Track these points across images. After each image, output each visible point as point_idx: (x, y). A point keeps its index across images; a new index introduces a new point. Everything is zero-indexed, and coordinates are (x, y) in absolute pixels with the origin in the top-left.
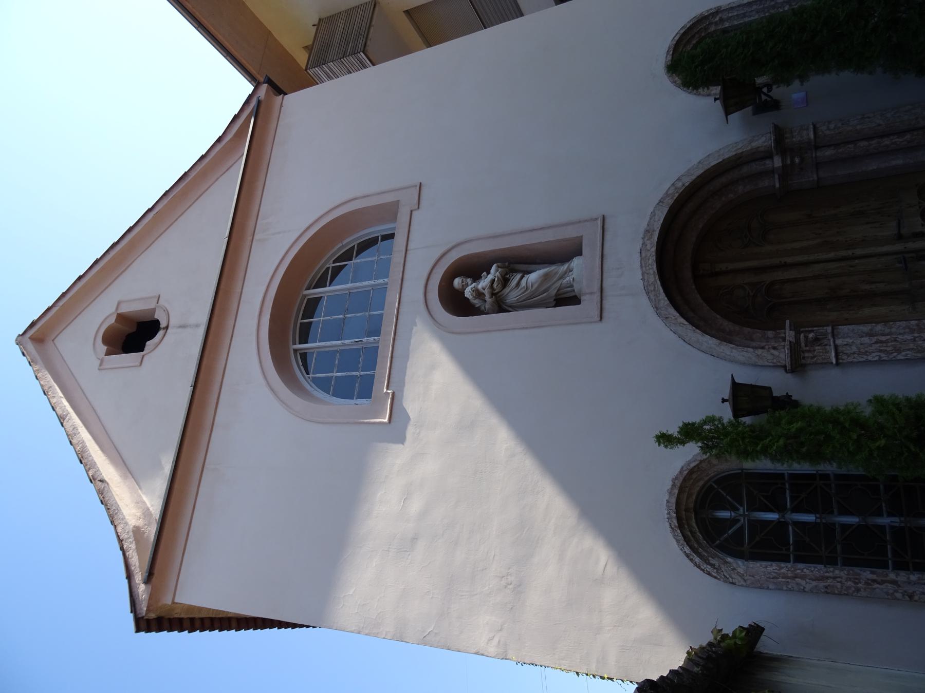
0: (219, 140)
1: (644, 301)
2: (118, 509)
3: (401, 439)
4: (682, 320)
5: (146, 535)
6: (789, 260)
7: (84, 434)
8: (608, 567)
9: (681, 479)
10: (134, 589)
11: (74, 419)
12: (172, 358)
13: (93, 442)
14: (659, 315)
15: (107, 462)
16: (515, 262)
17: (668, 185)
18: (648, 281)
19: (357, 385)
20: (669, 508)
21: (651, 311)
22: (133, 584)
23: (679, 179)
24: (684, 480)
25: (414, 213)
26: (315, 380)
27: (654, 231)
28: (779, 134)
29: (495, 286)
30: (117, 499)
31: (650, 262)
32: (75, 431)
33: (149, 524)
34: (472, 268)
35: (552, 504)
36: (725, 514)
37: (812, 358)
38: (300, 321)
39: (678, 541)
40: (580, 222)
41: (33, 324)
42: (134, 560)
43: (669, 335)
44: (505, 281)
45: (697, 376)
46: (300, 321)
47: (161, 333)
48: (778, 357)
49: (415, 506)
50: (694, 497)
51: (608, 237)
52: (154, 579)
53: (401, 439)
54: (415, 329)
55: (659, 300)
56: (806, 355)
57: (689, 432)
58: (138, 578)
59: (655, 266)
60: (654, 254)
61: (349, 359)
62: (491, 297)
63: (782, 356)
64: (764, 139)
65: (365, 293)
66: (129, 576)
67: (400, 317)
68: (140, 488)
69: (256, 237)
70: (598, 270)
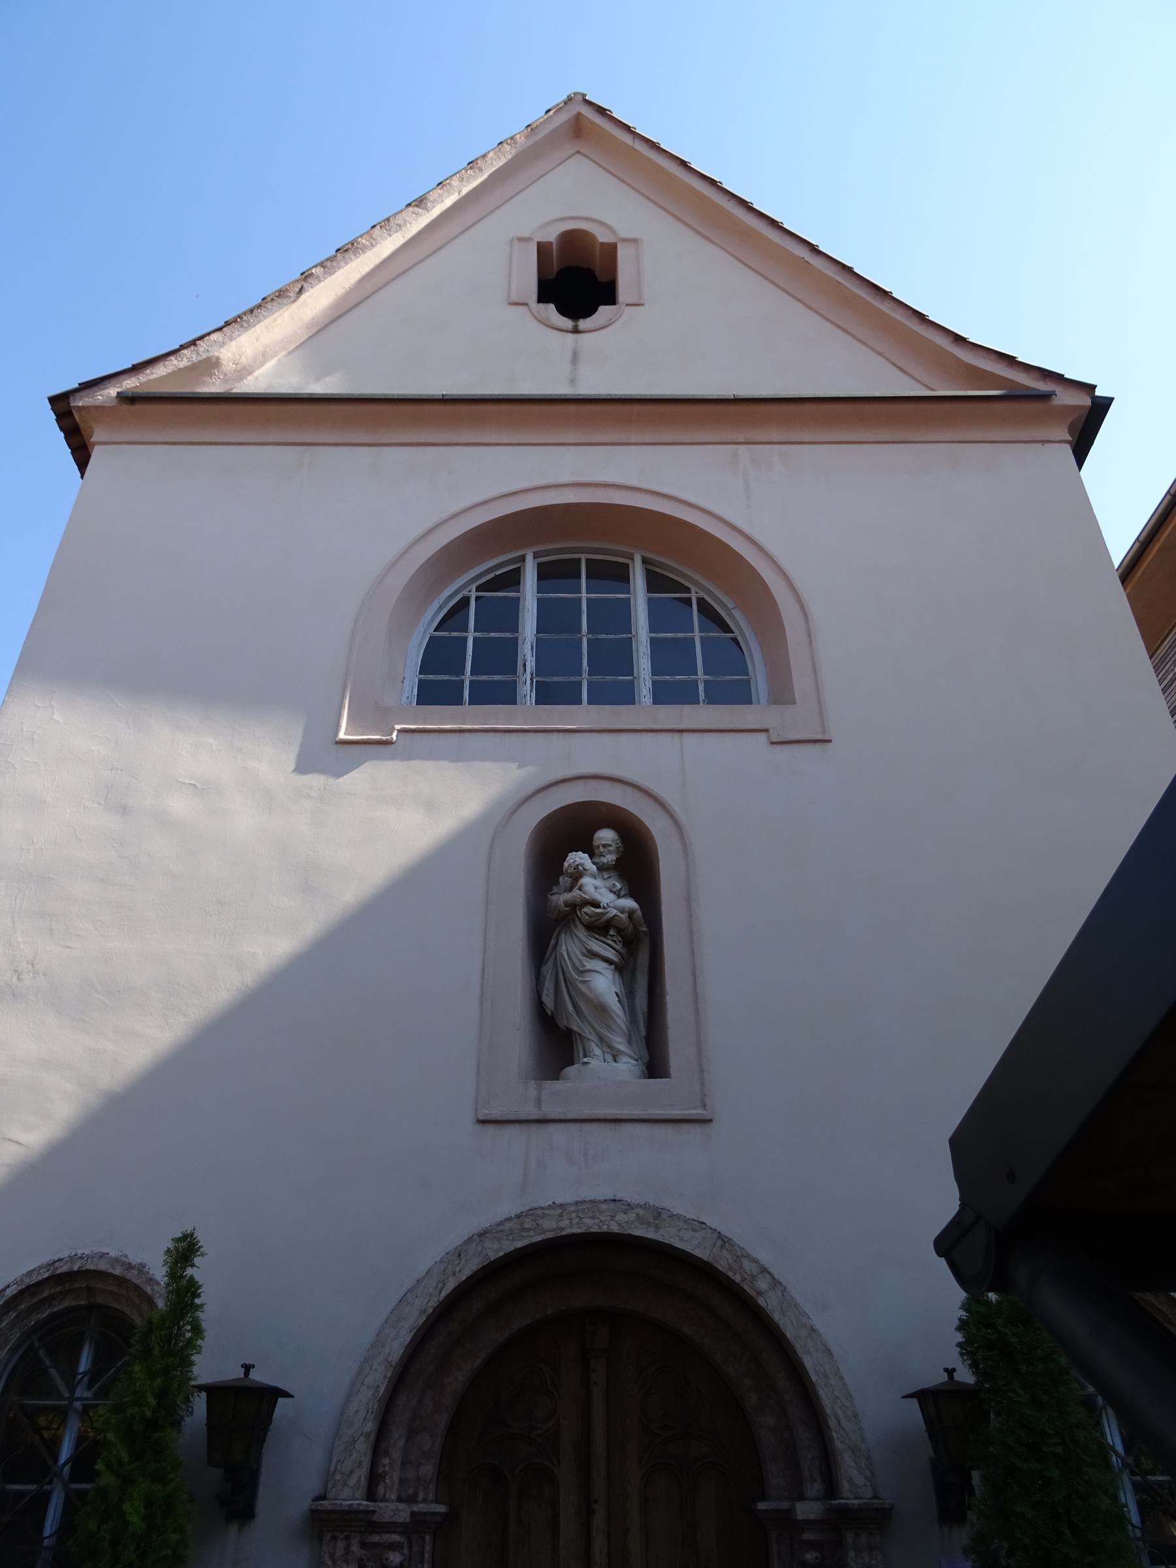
0: (959, 340)
1: (507, 1208)
2: (251, 326)
3: (304, 766)
4: (451, 1285)
5: (208, 379)
6: (599, 1520)
7: (388, 245)
8: (15, 1149)
9: (138, 1281)
10: (113, 381)
11: (418, 222)
12: (543, 355)
13: (377, 261)
14: (470, 1240)
15: (341, 292)
16: (639, 946)
17: (765, 1258)
18: (544, 1216)
19: (446, 677)
20: (71, 1259)
21: (482, 1221)
22: (122, 377)
23: (776, 1283)
24: (137, 1288)
25: (762, 737)
26: (465, 602)
27: (657, 1228)
28: (875, 1519)
29: (588, 909)
30: (266, 322)
31: (587, 1221)
32: (393, 229)
33: (225, 381)
34: (637, 866)
35: (137, 1042)
36: (84, 1364)
37: (332, 1556)
38: (583, 557)
39: (30, 1273)
40: (702, 1071)
41: (602, 111)
42: (161, 370)
43: (427, 1258)
44: (601, 927)
45: (314, 1310)
46: (583, 557)
47: (568, 323)
48: (345, 1484)
49: (179, 805)
50: (114, 1305)
51: (661, 1131)
52: (126, 407)
53: (304, 766)
54: (513, 766)
55: (499, 1240)
56: (341, 1545)
57: (185, 1294)
58: (130, 384)
59: (576, 1230)
60: (605, 1228)
61: (499, 655)
62: (566, 904)
63: (346, 1492)
64: (860, 1480)
66: (136, 369)
67: (541, 735)
68: (289, 353)
69: (742, 449)
70: (586, 1112)
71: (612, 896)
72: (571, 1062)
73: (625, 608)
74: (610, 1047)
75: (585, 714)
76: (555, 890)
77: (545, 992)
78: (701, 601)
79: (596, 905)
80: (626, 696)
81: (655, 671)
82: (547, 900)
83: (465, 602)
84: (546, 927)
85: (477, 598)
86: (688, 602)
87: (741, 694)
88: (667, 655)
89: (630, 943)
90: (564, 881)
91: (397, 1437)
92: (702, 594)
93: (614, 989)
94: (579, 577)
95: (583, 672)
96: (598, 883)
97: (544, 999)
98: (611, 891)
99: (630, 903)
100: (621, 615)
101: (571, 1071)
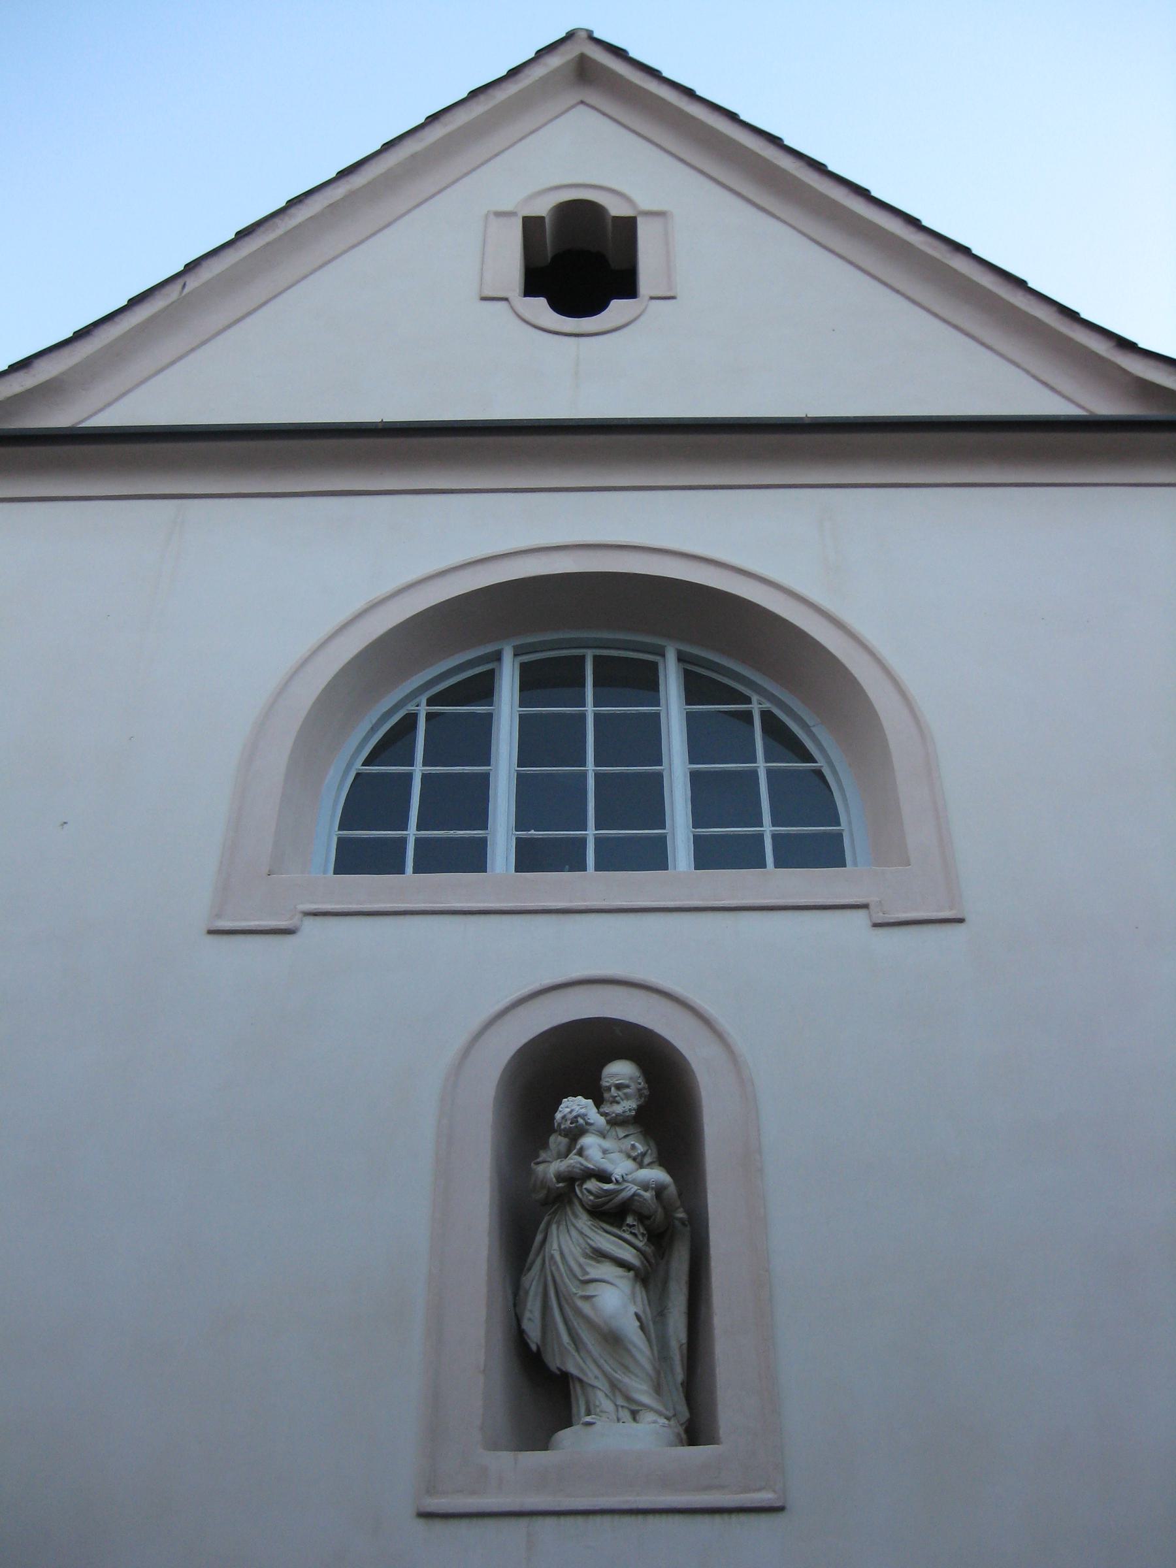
16: (670, 1238)
25: (860, 917)
26: (409, 722)
29: (592, 1185)
34: (668, 1114)
41: (619, 53)
44: (612, 1212)
61: (463, 802)
62: (560, 1177)
65: (653, 809)
71: (629, 1165)
72: (568, 1423)
73: (652, 728)
74: (628, 1399)
75: (591, 884)
76: (543, 1155)
77: (527, 1315)
78: (766, 716)
79: (603, 1177)
80: (653, 856)
81: (698, 820)
82: (530, 1172)
83: (409, 722)
84: (525, 1219)
85: (429, 716)
86: (747, 717)
87: (827, 852)
88: (717, 798)
89: (659, 1237)
90: (557, 1142)
91: (554, 61)
92: (767, 705)
93: (632, 1309)
94: (583, 685)
95: (590, 822)
96: (607, 1144)
97: (526, 1325)
98: (629, 1156)
99: (657, 1175)
100: (644, 740)
101: (565, 1436)
